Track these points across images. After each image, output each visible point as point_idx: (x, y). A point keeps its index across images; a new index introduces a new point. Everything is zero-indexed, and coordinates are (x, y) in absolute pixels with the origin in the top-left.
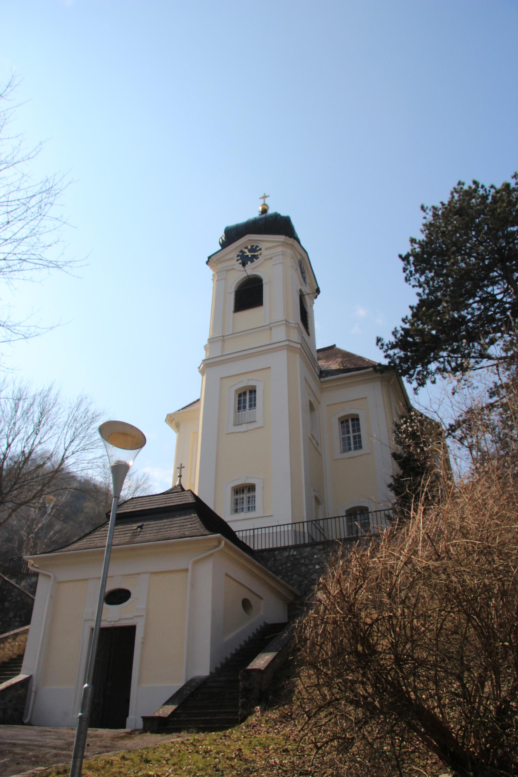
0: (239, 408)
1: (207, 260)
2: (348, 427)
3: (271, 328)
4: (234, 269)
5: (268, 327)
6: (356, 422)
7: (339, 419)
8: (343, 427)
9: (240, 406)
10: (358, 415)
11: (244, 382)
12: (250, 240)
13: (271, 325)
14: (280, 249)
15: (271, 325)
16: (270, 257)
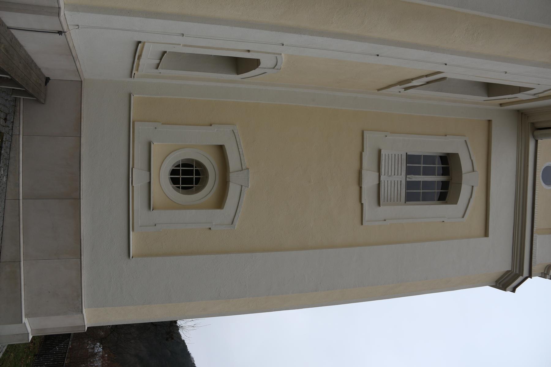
0: (410, 159)
9: (413, 163)
10: (455, 202)
11: (470, 181)
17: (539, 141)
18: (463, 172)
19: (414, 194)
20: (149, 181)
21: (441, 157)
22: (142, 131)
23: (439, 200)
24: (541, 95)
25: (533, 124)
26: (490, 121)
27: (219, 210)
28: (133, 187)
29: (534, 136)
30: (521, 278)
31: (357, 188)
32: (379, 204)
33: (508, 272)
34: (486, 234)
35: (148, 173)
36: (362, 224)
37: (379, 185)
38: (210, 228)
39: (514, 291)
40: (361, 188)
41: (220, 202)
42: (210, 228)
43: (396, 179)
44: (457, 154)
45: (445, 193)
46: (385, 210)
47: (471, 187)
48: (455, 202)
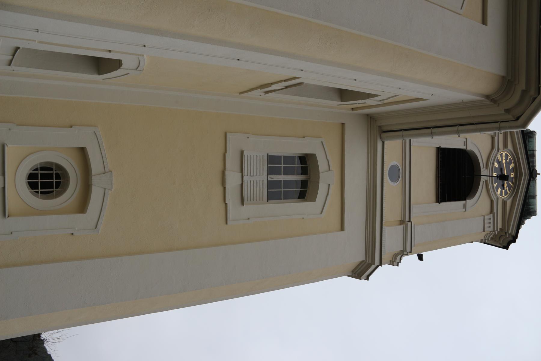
0: (271, 159)
2: (287, 172)
3: (402, 222)
4: (493, 148)
5: (407, 220)
6: (297, 189)
7: (313, 156)
8: (288, 159)
9: (274, 163)
10: (314, 200)
11: (327, 179)
14: (500, 226)
15: (409, 224)
16: (495, 211)
17: (385, 142)
18: (320, 171)
19: (275, 193)
20: (3, 186)
21: (300, 157)
23: (299, 198)
26: (343, 124)
27: (81, 215)
29: (381, 138)
30: (373, 267)
32: (242, 203)
33: (362, 262)
34: (342, 229)
36: (227, 223)
37: (242, 185)
38: (72, 234)
39: (367, 279)
40: (224, 188)
41: (82, 206)
42: (72, 234)
43: (258, 179)
45: (304, 192)
46: (249, 209)
47: (327, 186)
48: (314, 200)
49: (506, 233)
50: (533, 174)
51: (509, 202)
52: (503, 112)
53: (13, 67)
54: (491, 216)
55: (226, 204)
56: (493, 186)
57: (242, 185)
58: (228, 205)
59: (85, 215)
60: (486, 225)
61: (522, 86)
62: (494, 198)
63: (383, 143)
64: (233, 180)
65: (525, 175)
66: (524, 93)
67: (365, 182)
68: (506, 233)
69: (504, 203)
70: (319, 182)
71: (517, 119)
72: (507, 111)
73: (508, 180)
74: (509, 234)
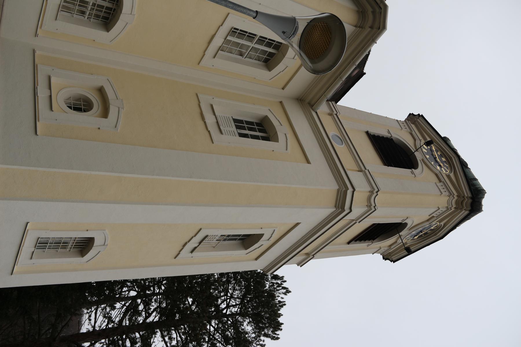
1: (416, 113)
3: (361, 171)
4: (415, 140)
5: (363, 169)
12: (451, 158)
13: (367, 171)
17: (318, 111)
20: (50, 94)
22: (43, 71)
24: (341, 149)
25: (309, 103)
26: (281, 102)
28: (38, 97)
29: (313, 110)
31: (202, 123)
33: (338, 190)
35: (49, 91)
36: (213, 143)
37: (217, 122)
38: (99, 128)
40: (205, 122)
41: (105, 114)
42: (99, 128)
44: (108, 32)
46: (225, 138)
47: (284, 135)
49: (463, 197)
50: (464, 165)
51: (452, 175)
52: (370, 29)
53: (33, 261)
54: (441, 184)
55: (209, 131)
56: (431, 164)
57: (217, 122)
58: (211, 132)
59: (107, 33)
60: (442, 190)
61: (370, 10)
62: (437, 172)
63: (316, 112)
64: (210, 119)
65: (454, 158)
66: (374, 12)
67: (314, 137)
68: (463, 197)
69: (448, 176)
70: (276, 132)
71: (379, 28)
72: (371, 27)
73: (433, 143)
74: (467, 197)
